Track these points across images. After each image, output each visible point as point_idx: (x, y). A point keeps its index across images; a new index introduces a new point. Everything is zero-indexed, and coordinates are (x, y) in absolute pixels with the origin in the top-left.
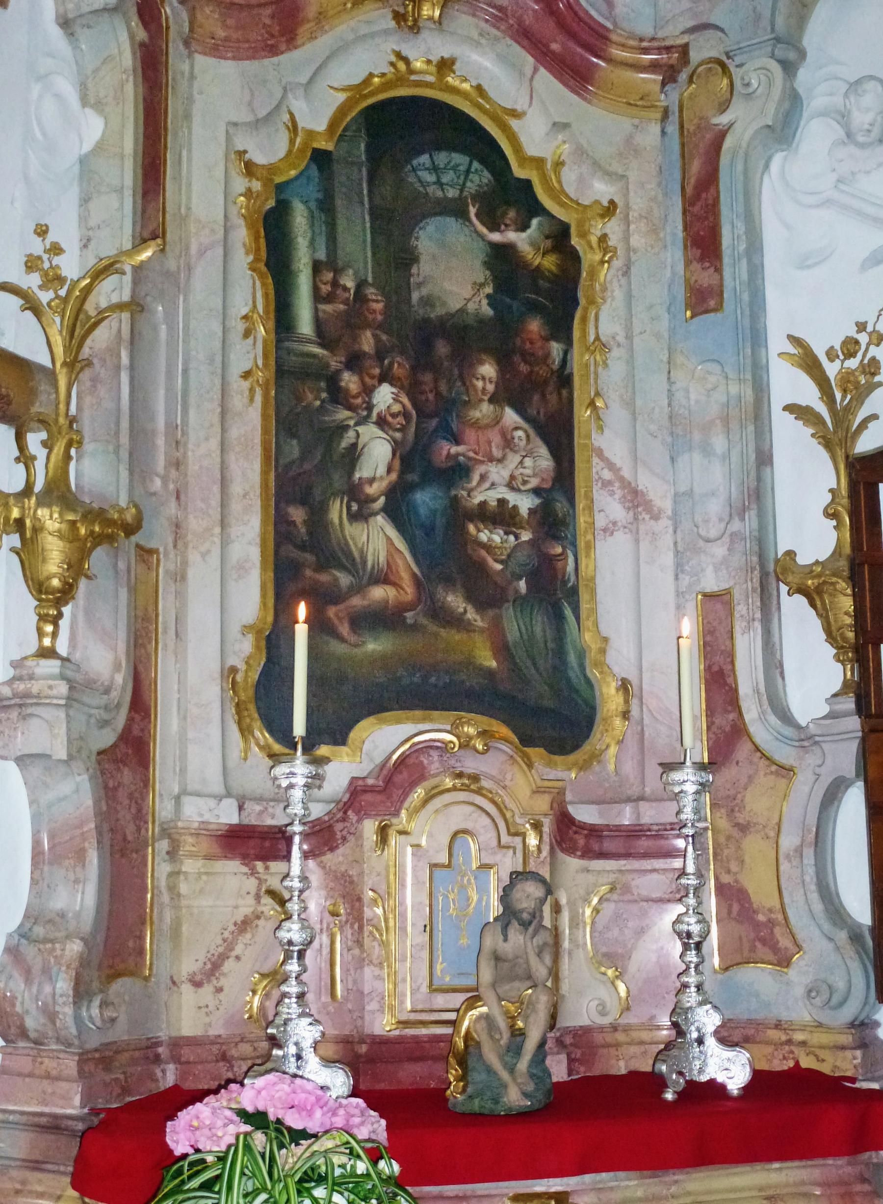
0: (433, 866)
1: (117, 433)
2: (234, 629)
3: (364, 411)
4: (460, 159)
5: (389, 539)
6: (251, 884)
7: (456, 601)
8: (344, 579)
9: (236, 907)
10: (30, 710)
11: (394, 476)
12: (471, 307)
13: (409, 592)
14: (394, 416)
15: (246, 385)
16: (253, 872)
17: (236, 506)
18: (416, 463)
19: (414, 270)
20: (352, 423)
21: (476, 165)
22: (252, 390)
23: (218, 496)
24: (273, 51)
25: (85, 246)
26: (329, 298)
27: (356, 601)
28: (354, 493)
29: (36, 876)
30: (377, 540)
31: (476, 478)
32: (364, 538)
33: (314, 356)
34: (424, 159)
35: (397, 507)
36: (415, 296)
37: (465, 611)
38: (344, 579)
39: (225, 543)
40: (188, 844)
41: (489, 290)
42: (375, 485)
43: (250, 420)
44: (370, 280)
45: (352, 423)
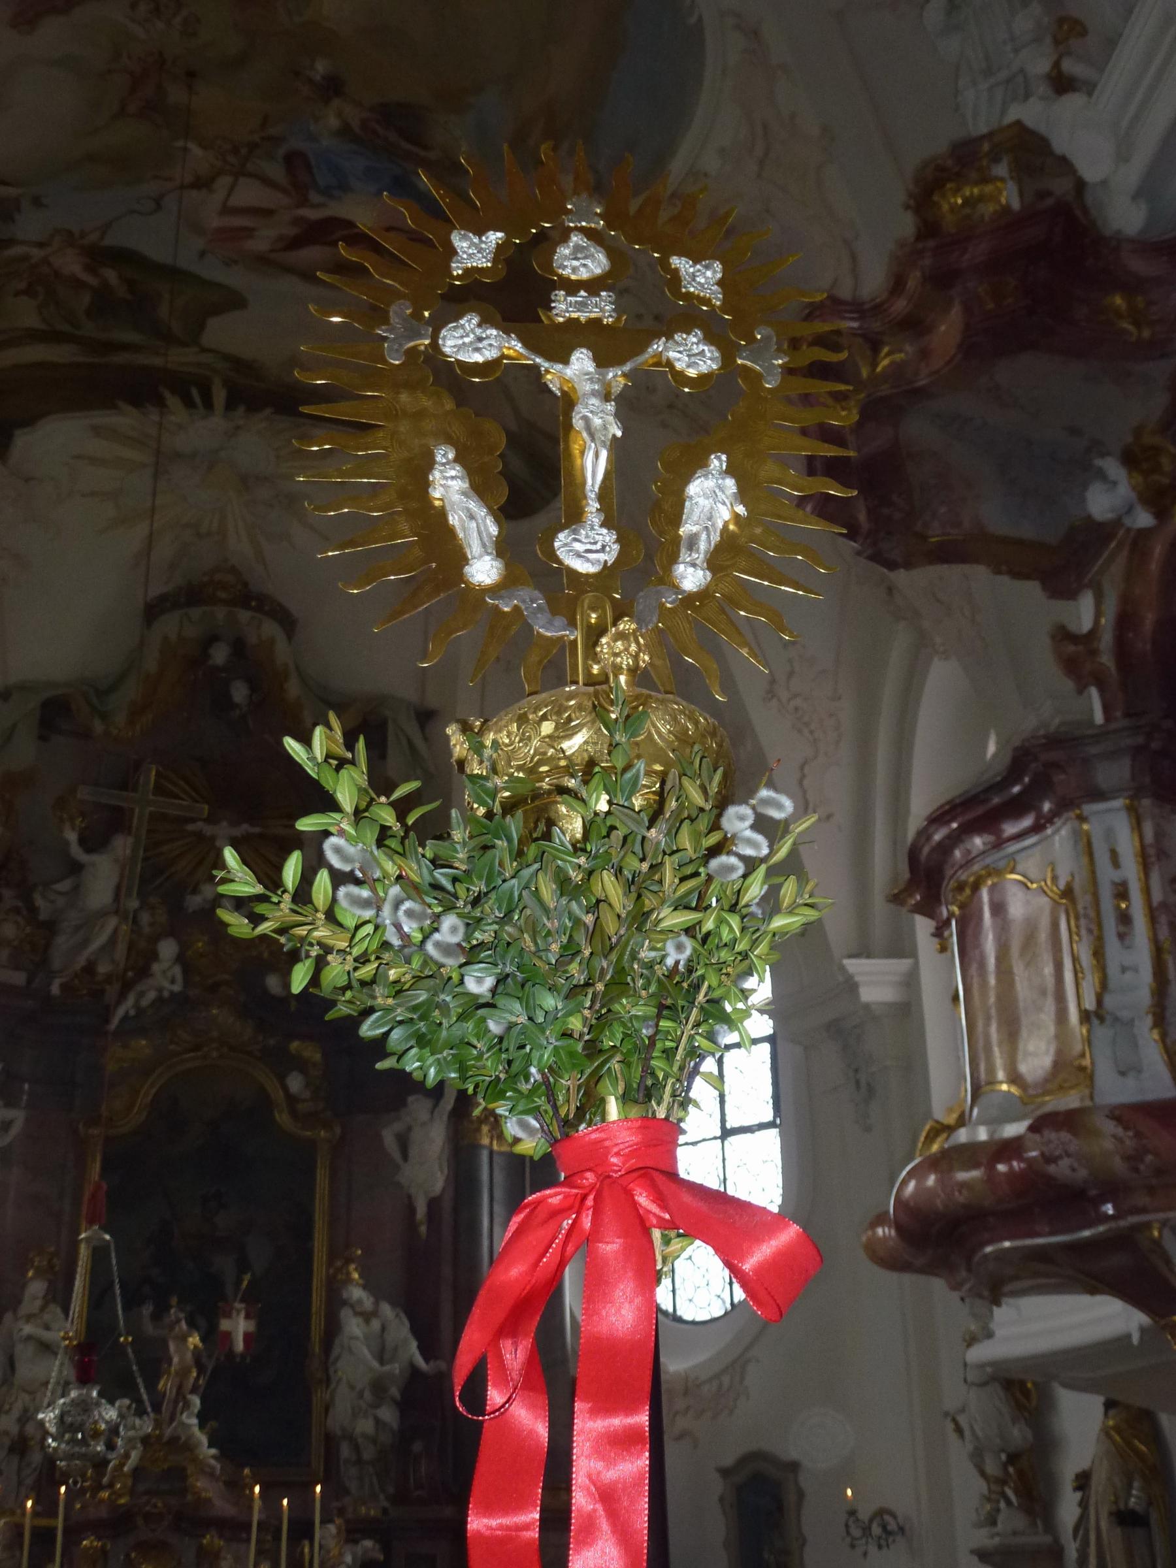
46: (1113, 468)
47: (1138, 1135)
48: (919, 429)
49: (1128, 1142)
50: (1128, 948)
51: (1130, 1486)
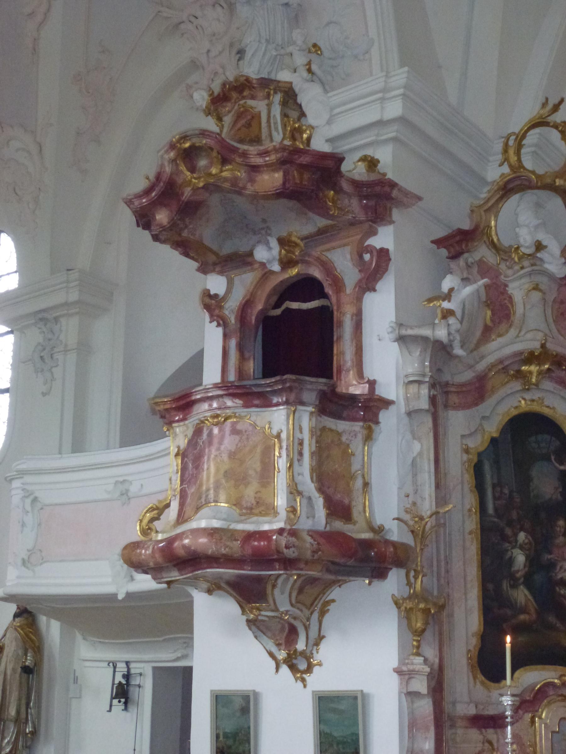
0: (553, 732)
1: (432, 566)
2: (470, 634)
3: (514, 543)
4: (546, 437)
5: (525, 595)
6: (481, 737)
7: (552, 619)
8: (509, 612)
9: (476, 747)
10: (413, 676)
11: (527, 569)
12: (554, 497)
13: (534, 616)
14: (526, 544)
15: (470, 536)
16: (482, 733)
17: (469, 586)
18: (533, 562)
19: (531, 484)
20: (510, 548)
21: (553, 439)
22: (472, 538)
23: (463, 583)
24: (477, 405)
25: (416, 493)
26: (499, 498)
27: (514, 621)
28: (512, 577)
29: (411, 735)
30: (522, 595)
31: (558, 568)
32: (516, 594)
33: (494, 522)
34: (533, 439)
35: (528, 582)
36: (532, 494)
37: (556, 623)
38: (509, 612)
39: (466, 600)
40: (459, 723)
41: (560, 490)
42: (520, 573)
43: (473, 549)
44: (515, 490)
45: (510, 548)
46: (274, 243)
47: (318, 544)
48: (214, 200)
49: (315, 546)
50: (301, 466)
51: (26, 655)
